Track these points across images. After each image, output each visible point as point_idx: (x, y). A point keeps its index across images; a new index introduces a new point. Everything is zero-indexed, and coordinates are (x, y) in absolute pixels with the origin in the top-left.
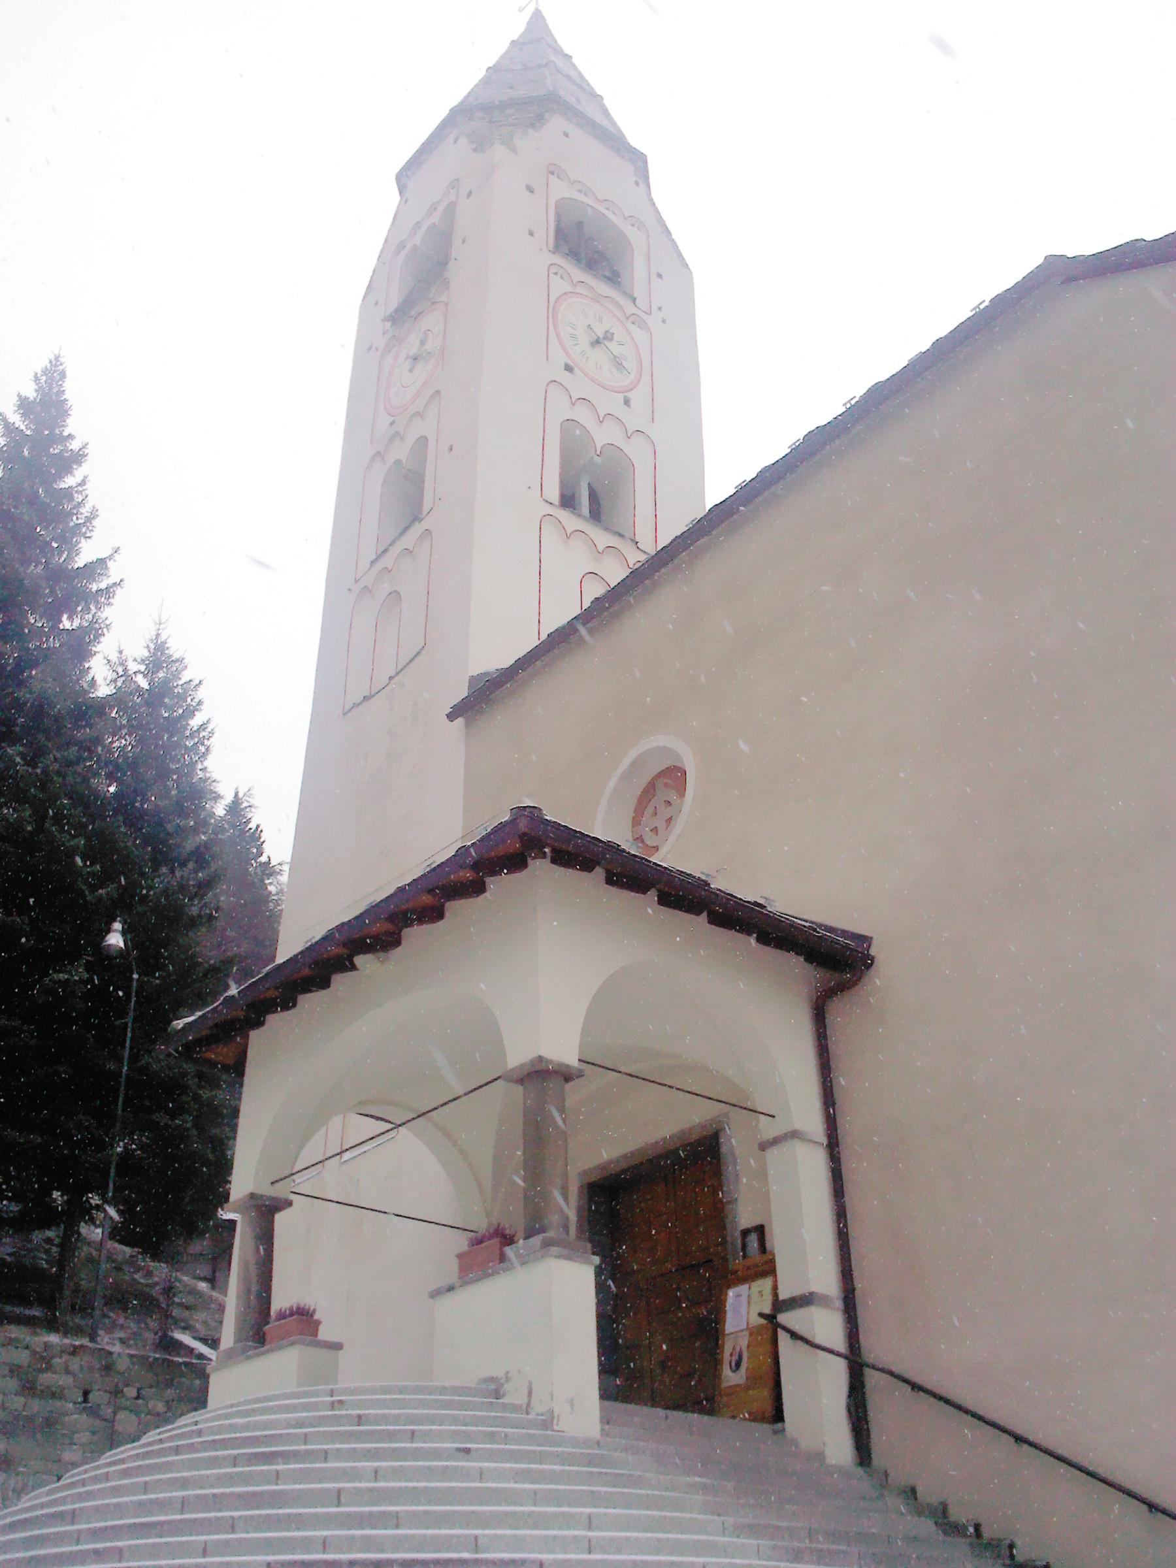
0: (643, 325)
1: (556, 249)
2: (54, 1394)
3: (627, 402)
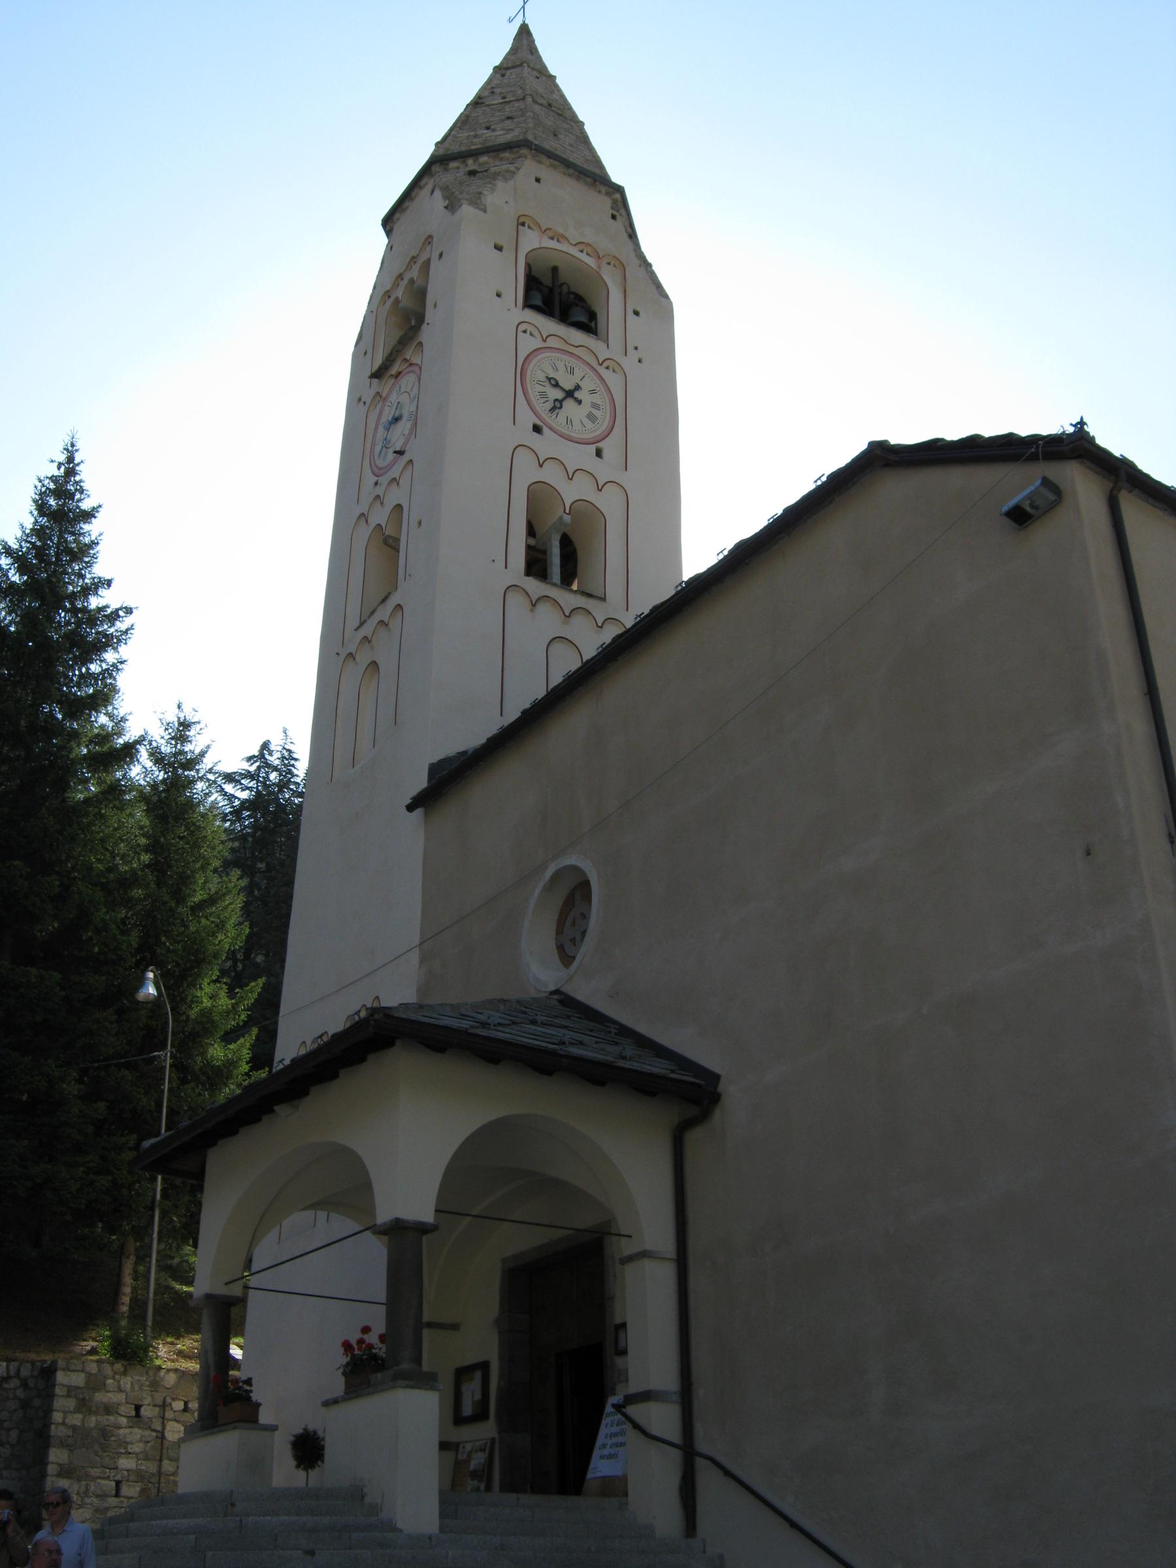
0: (616, 368)
1: (528, 305)
2: (109, 1409)
3: (599, 453)
